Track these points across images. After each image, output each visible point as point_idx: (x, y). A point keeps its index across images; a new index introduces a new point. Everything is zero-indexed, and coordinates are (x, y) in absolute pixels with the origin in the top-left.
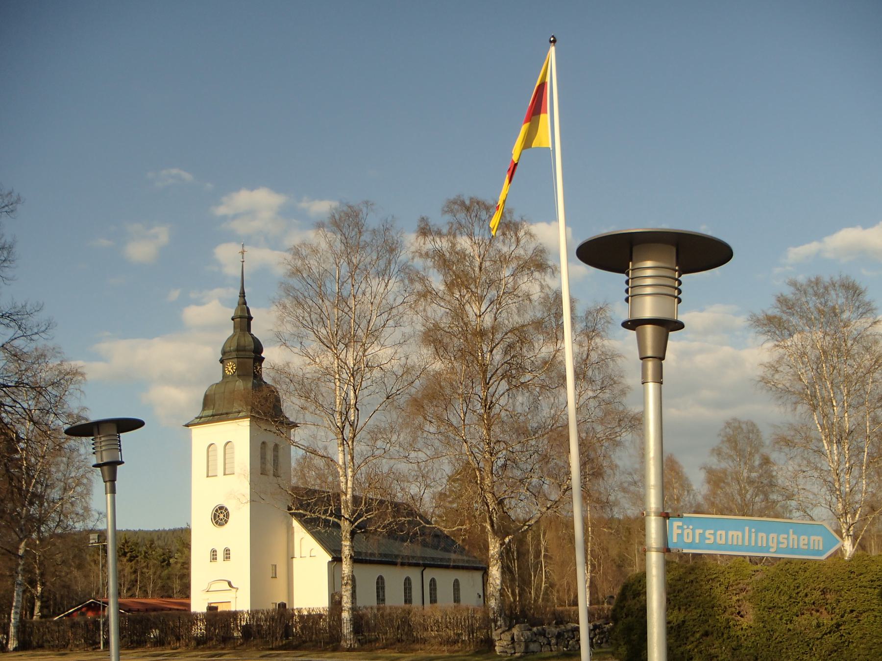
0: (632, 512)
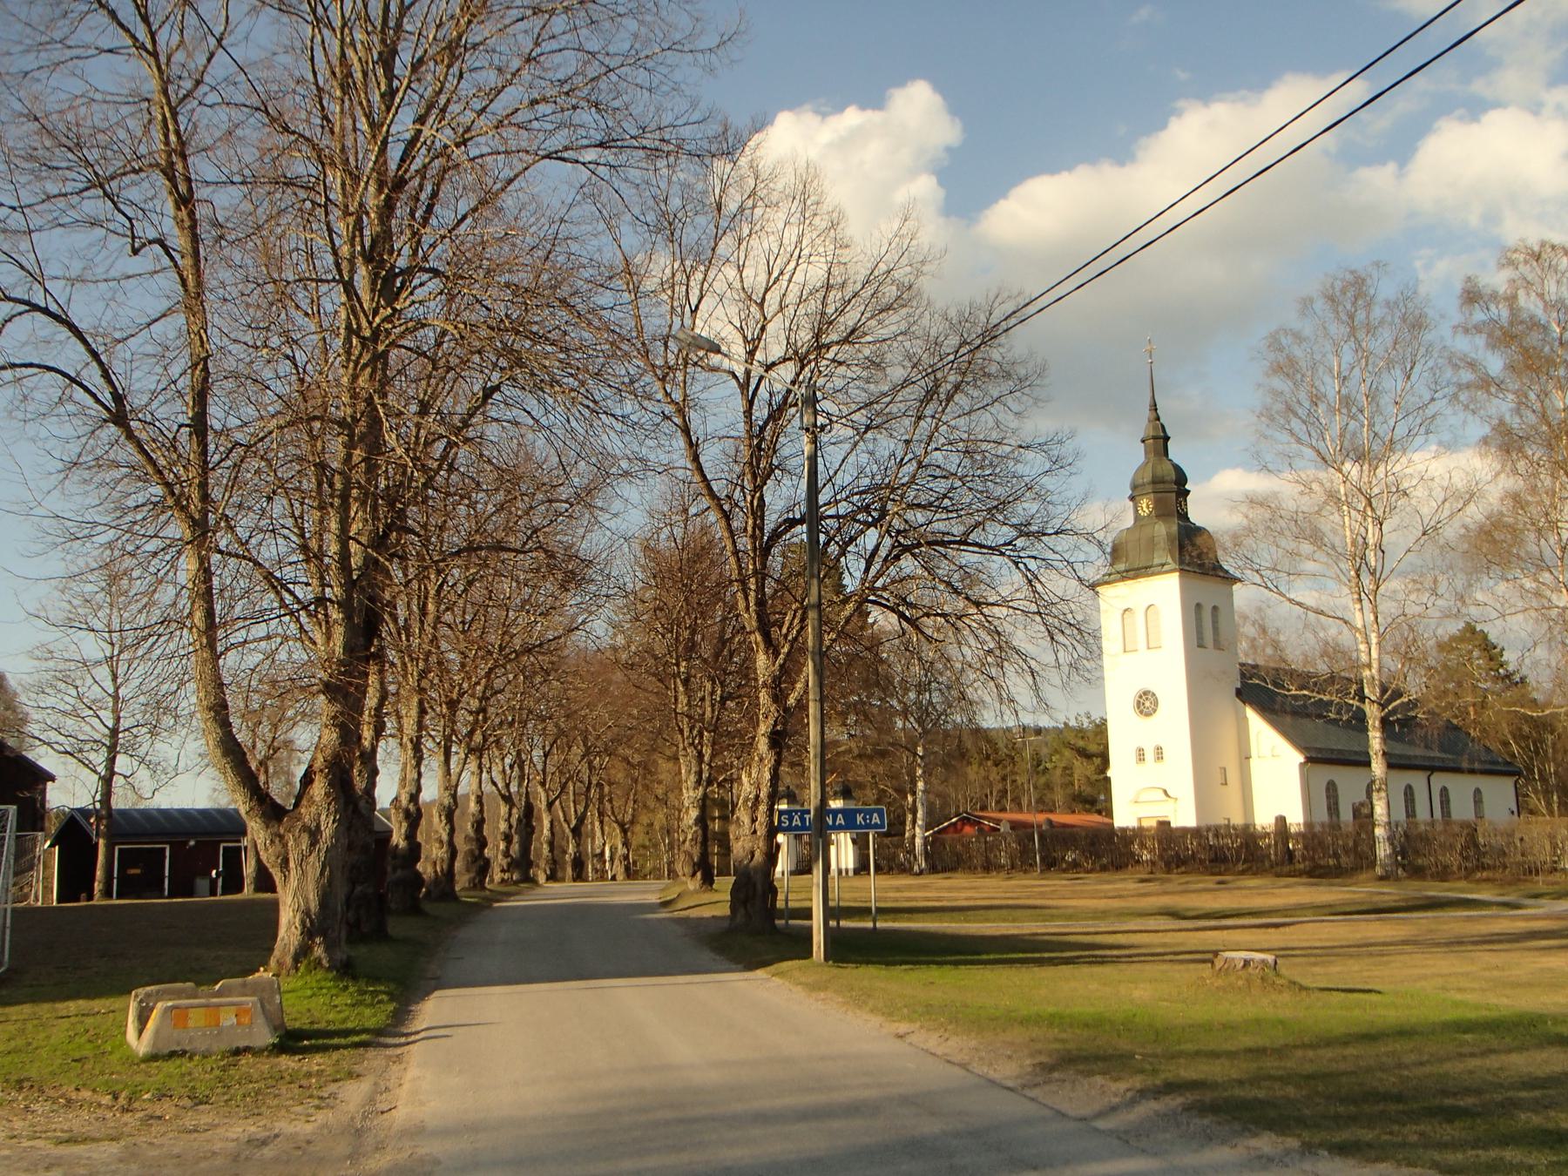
0: (1064, 711)
